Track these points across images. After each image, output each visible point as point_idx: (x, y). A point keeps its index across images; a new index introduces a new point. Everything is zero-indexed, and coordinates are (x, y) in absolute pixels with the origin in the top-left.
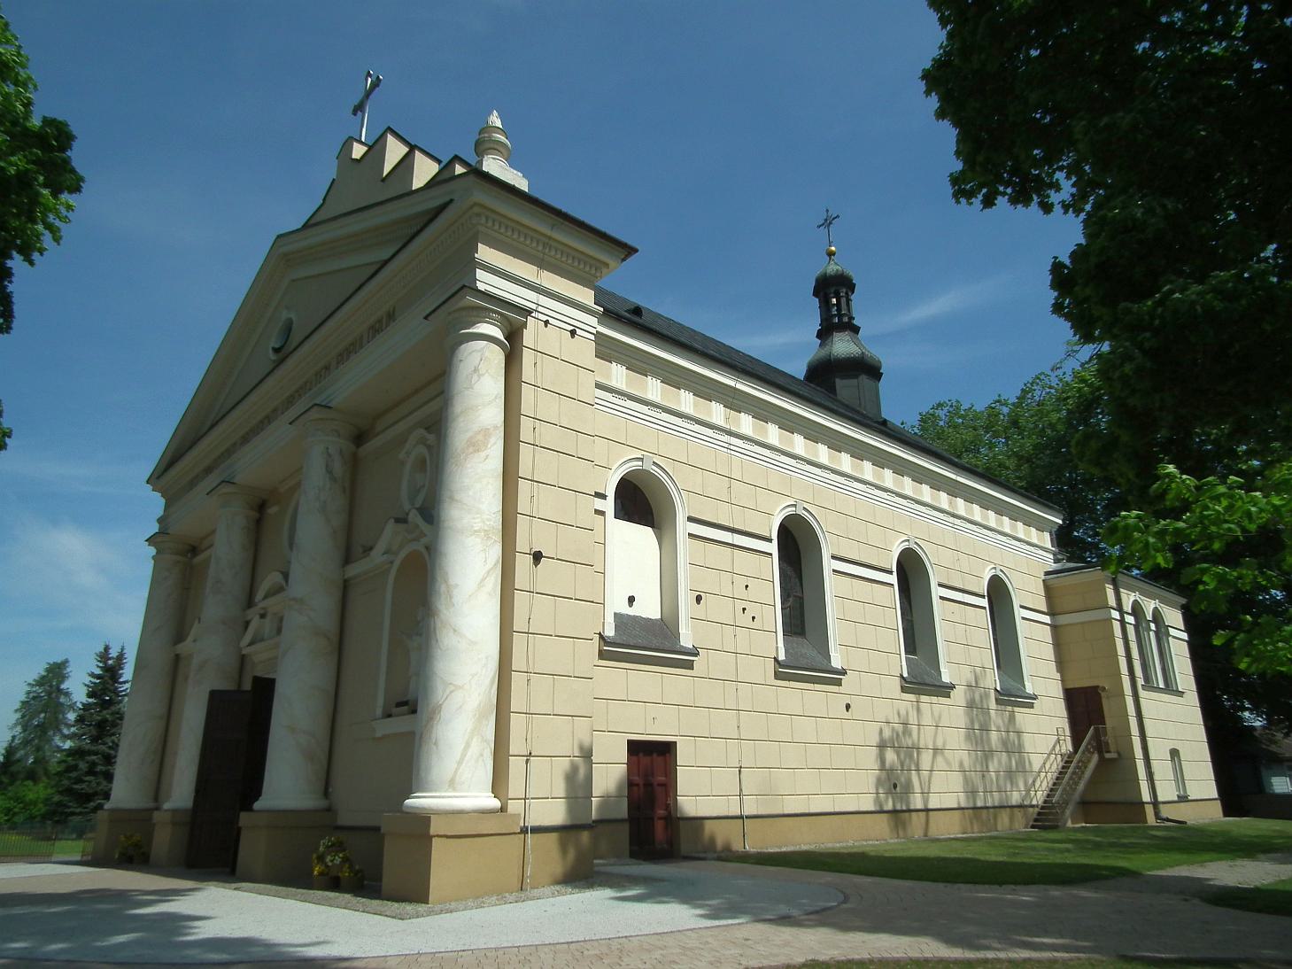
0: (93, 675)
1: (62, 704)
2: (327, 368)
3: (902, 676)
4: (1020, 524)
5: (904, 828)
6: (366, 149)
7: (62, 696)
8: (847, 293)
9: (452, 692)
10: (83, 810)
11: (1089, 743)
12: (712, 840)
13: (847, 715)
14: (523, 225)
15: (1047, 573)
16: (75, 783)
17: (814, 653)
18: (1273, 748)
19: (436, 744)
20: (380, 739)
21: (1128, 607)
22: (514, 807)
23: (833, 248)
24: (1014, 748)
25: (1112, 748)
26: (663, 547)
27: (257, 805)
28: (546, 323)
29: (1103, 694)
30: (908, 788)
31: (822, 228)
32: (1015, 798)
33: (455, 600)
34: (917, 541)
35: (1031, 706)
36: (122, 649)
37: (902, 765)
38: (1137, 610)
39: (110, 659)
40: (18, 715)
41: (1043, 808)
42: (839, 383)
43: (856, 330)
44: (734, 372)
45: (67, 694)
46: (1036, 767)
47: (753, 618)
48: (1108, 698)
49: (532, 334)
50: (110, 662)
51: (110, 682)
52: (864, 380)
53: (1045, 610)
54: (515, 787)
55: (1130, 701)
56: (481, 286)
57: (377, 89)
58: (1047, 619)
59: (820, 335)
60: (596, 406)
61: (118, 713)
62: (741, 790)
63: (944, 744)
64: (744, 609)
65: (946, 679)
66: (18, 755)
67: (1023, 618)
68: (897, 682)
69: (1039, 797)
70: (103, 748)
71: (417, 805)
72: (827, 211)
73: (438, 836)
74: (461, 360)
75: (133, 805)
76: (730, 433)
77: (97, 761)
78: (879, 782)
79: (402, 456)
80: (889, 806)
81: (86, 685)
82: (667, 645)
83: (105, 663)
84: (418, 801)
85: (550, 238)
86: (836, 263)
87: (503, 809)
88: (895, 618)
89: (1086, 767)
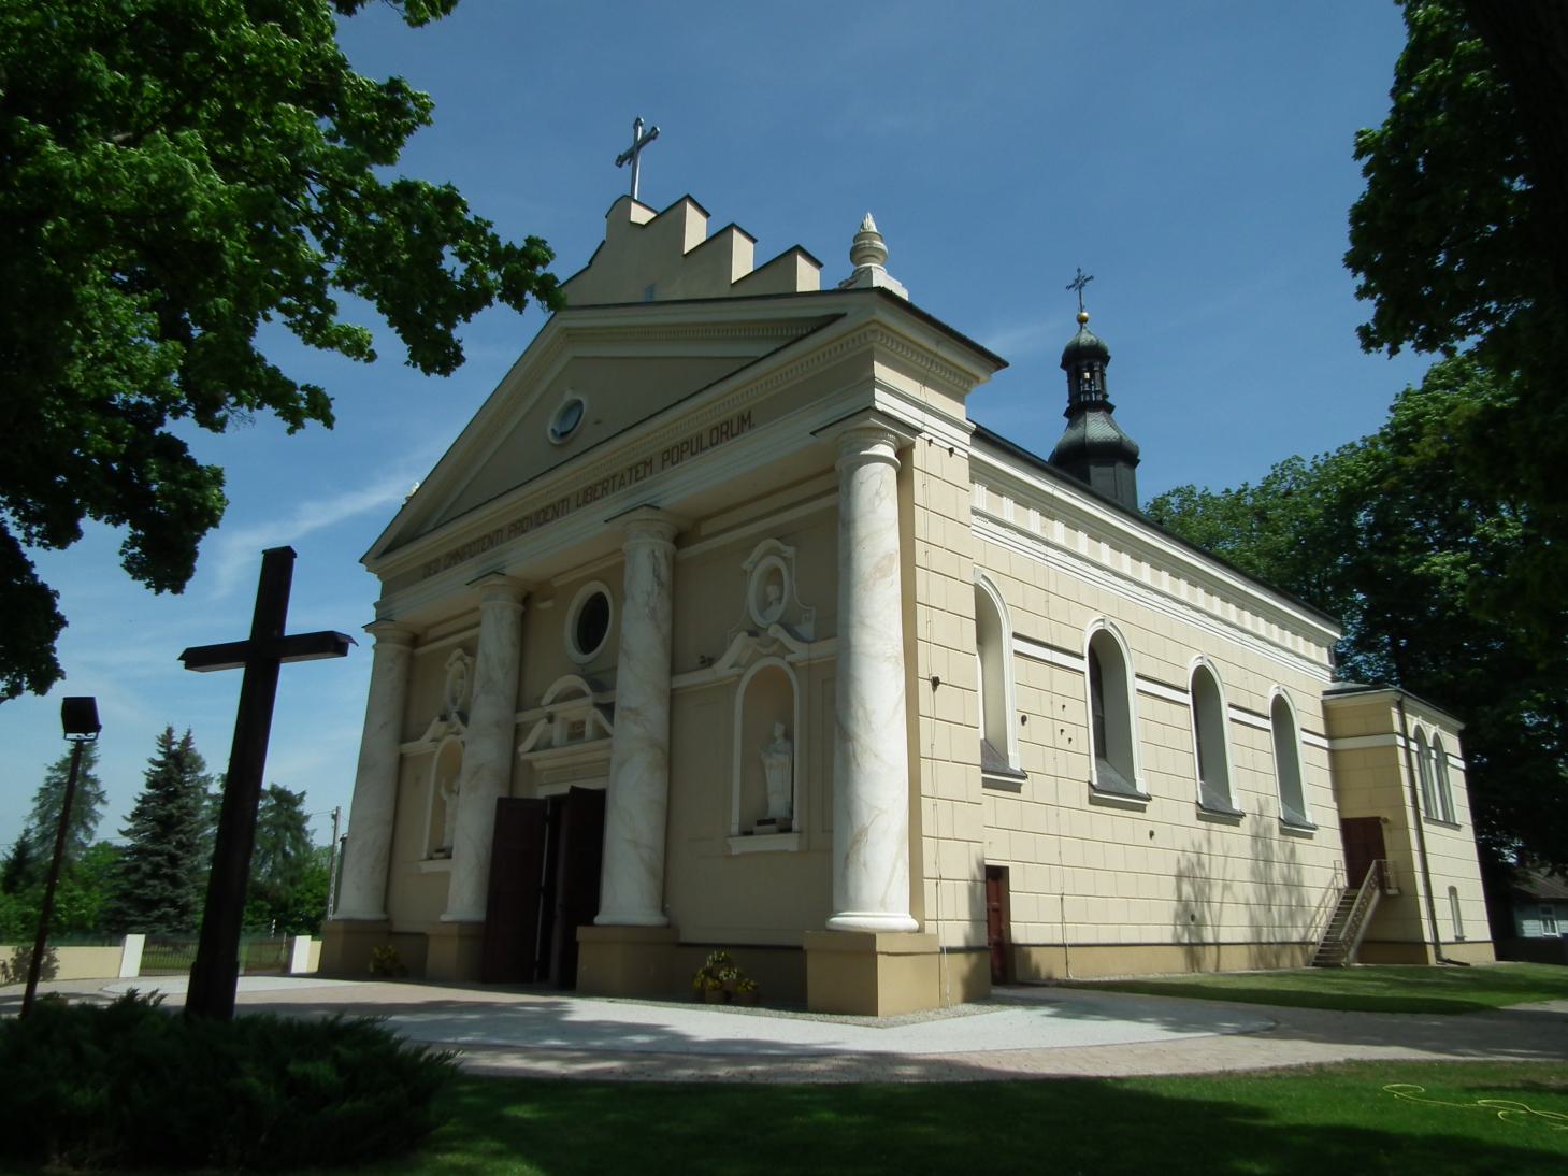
0: (153, 762)
1: (88, 793)
2: (648, 464)
3: (1197, 803)
4: (1300, 639)
5: (1198, 965)
6: (653, 215)
7: (89, 785)
8: (1101, 367)
9: (878, 815)
10: (146, 919)
11: (1371, 878)
12: (1038, 970)
13: (1150, 842)
14: (911, 341)
15: (1326, 693)
16: (137, 888)
17: (1123, 782)
18: (1525, 887)
19: (865, 865)
20: (737, 856)
21: (1411, 734)
22: (930, 927)
23: (1085, 314)
24: (1293, 885)
25: (1393, 885)
26: (985, 666)
27: (598, 920)
28: (930, 441)
29: (1384, 826)
30: (1201, 924)
31: (1072, 289)
32: (1295, 937)
33: (874, 726)
34: (1211, 658)
35: (1310, 836)
36: (189, 733)
37: (1196, 897)
38: (1420, 736)
39: (174, 743)
40: (36, 805)
41: (1323, 945)
42: (1094, 470)
43: (1109, 409)
44: (1052, 478)
45: (94, 782)
46: (1315, 903)
47: (1070, 740)
48: (1390, 830)
49: (920, 454)
50: (174, 747)
51: (176, 770)
52: (1121, 467)
53: (1323, 733)
54: (930, 913)
55: (1413, 834)
56: (879, 406)
57: (652, 142)
58: (1325, 743)
59: (1068, 414)
60: (973, 527)
61: (185, 808)
62: (1063, 917)
63: (1234, 876)
64: (1062, 731)
65: (1236, 806)
66: (34, 852)
67: (1305, 742)
68: (1192, 810)
69: (1316, 935)
70: (170, 848)
71: (851, 923)
72: (1079, 270)
73: (882, 953)
74: (861, 483)
75: (367, 916)
76: (1047, 543)
77: (163, 862)
78: (1177, 916)
79: (746, 565)
80: (1186, 940)
81: (146, 774)
82: (1000, 768)
83: (169, 749)
84: (844, 920)
85: (936, 355)
86: (1089, 332)
87: (920, 930)
88: (1189, 740)
89: (1368, 903)
